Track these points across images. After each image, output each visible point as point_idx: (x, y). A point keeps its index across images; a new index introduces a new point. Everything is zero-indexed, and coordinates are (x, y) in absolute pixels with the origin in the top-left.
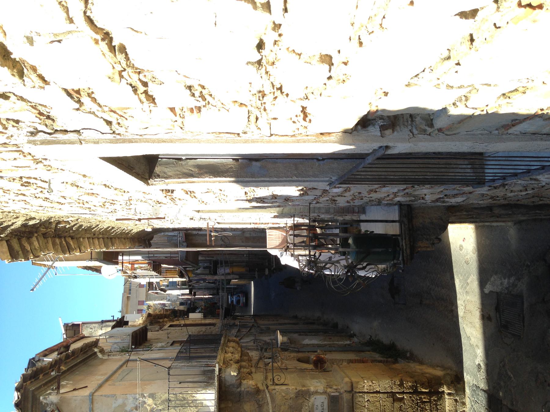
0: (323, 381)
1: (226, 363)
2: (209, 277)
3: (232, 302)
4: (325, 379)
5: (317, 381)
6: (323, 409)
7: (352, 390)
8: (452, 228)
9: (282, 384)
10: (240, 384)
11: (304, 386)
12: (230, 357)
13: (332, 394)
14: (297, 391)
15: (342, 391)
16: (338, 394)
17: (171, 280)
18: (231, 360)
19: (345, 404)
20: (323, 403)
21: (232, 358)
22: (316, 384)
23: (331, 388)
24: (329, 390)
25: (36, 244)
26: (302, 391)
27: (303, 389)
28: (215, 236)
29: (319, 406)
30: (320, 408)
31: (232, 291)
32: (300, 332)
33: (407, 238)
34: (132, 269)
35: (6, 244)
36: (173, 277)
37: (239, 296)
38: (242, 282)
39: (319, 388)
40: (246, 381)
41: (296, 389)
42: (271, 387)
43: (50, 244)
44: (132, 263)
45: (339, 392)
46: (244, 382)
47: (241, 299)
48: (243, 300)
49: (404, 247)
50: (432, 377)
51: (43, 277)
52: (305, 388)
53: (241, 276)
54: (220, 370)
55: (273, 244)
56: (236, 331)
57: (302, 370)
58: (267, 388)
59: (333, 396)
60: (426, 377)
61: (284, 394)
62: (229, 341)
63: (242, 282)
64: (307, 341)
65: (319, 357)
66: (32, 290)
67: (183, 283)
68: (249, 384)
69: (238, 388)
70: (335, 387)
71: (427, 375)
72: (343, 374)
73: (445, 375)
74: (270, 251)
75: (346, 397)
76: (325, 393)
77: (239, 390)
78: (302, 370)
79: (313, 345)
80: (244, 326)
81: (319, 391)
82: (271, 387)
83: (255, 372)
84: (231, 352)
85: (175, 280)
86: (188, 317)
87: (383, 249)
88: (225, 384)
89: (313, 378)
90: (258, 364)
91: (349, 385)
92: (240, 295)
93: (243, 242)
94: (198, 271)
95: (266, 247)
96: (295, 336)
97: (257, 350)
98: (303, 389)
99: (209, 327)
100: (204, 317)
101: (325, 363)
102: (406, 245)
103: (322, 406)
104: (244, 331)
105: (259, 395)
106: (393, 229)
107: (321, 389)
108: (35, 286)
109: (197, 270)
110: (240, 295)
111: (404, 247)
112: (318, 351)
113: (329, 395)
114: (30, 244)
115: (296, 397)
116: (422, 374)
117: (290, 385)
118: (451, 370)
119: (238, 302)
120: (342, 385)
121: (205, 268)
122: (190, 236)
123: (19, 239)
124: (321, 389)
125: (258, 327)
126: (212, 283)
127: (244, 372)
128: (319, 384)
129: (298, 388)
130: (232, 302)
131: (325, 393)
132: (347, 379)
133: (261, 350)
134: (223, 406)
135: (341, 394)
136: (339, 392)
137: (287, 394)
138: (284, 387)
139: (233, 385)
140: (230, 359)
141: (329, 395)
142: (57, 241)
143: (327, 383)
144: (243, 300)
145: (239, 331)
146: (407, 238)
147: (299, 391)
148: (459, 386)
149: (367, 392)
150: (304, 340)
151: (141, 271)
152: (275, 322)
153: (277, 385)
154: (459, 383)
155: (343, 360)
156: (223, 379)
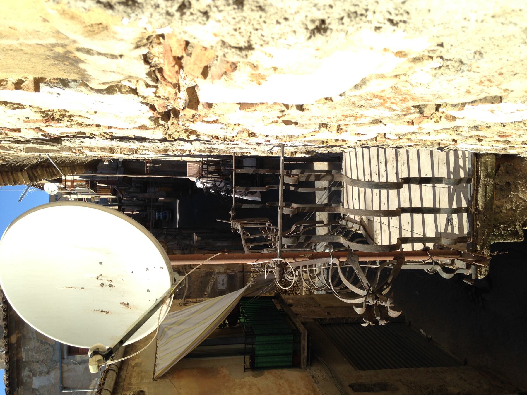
2: (141, 196)
3: (159, 217)
8: (326, 163)
15: (237, 271)
17: (102, 197)
23: (229, 270)
24: (228, 271)
25: (39, 172)
30: (221, 283)
31: (160, 208)
34: (71, 187)
35: (26, 173)
36: (104, 195)
37: (166, 213)
38: (168, 200)
43: (45, 172)
44: (72, 181)
47: (168, 215)
48: (169, 216)
51: (26, 192)
53: (168, 196)
59: (231, 275)
61: (197, 274)
63: (168, 200)
64: (219, 244)
66: (20, 201)
67: (113, 200)
74: (190, 178)
75: (239, 275)
76: (225, 273)
79: (223, 247)
85: (106, 197)
92: (167, 212)
93: (377, 250)
94: (131, 190)
95: (186, 174)
103: (223, 281)
108: (21, 199)
109: (129, 189)
110: (167, 212)
114: (37, 172)
119: (165, 217)
121: (136, 187)
122: (129, 165)
123: (32, 170)
126: (141, 200)
130: (159, 217)
131: (225, 273)
133: (183, 250)
135: (236, 273)
142: (48, 169)
144: (169, 216)
149: (253, 272)
151: (79, 189)
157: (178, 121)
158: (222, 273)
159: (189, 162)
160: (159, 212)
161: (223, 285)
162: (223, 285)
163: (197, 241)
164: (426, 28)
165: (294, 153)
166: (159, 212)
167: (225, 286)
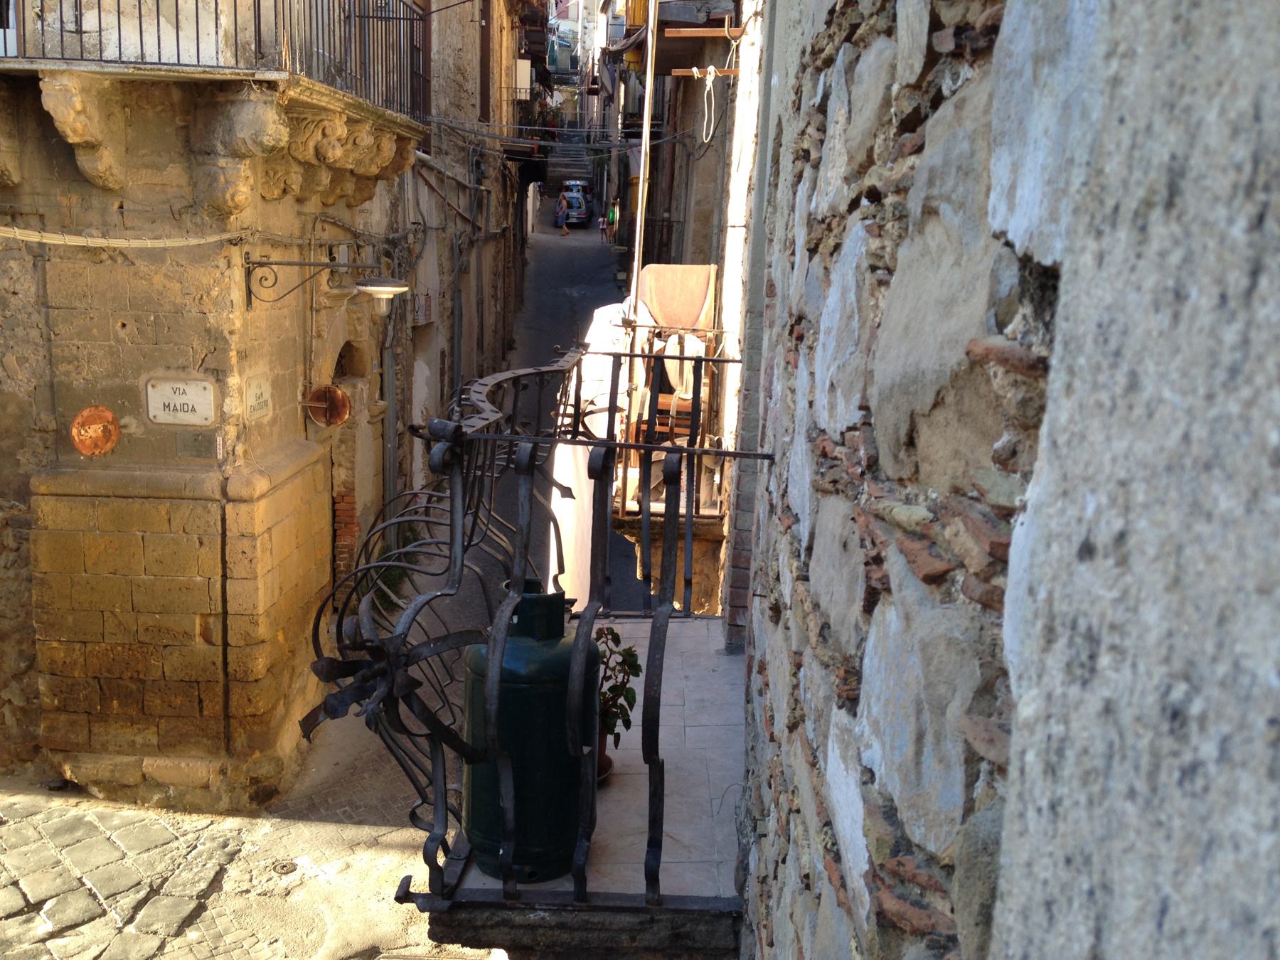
0: (268, 415)
1: (295, 114)
3: (569, 189)
4: (274, 421)
5: (267, 396)
6: (175, 409)
7: (229, 501)
9: (249, 292)
10: (237, 155)
11: (243, 356)
12: (334, 130)
13: (219, 440)
14: (226, 333)
15: (229, 469)
16: (220, 457)
18: (324, 135)
19: (188, 476)
20: (193, 410)
21: (333, 139)
22: (250, 395)
23: (238, 438)
24: (232, 431)
26: (226, 351)
27: (233, 354)
28: (702, 81)
29: (183, 399)
30: (178, 400)
32: (452, 354)
33: (565, 937)
39: (236, 401)
40: (249, 173)
41: (231, 333)
42: (236, 255)
45: (225, 460)
46: (244, 168)
49: (518, 918)
50: (273, 724)
52: (234, 360)
54: (272, 85)
55: (659, 288)
56: (459, 178)
57: (308, 357)
58: (230, 241)
60: (274, 708)
61: (215, 293)
62: (401, 140)
65: (344, 406)
68: (242, 184)
69: (224, 144)
70: (240, 449)
71: (280, 709)
72: (284, 475)
73: (279, 763)
77: (220, 148)
78: (308, 357)
80: (479, 203)
81: (227, 401)
82: (236, 255)
83: (299, 213)
84: (343, 138)
86: (522, 57)
87: (510, 815)
88: (232, 102)
89: (276, 384)
90: (334, 224)
91: (244, 493)
93: (698, 203)
96: (440, 341)
97: (392, 227)
98: (233, 354)
99: (477, 101)
100: (520, 102)
101: (329, 423)
102: (532, 927)
103: (184, 408)
104: (461, 203)
105: (211, 215)
106: (619, 875)
107: (233, 406)
111: (518, 918)
112: (381, 403)
113: (217, 429)
115: (208, 331)
116: (286, 697)
117: (250, 315)
118: (297, 775)
120: (245, 471)
124: (233, 406)
125: (472, 243)
127: (287, 173)
128: (252, 401)
129: (235, 338)
130: (569, 189)
131: (223, 418)
132: (262, 485)
134: (176, 95)
136: (225, 460)
137: (215, 302)
138: (237, 295)
139: (231, 130)
140: (328, 131)
141: (217, 429)
143: (259, 426)
145: (461, 187)
146: (565, 937)
147: (226, 342)
148: (246, 797)
150: (428, 364)
152: (488, 290)
153: (248, 273)
154: (252, 798)
155: (352, 469)
156: (243, 95)
157: (1229, 202)
158: (219, 406)
159: (719, 276)
160: (585, 190)
161: (166, 406)
162: (166, 406)
163: (370, 296)
164: (1051, 918)
165: (619, 22)
166: (585, 190)
167: (163, 417)
